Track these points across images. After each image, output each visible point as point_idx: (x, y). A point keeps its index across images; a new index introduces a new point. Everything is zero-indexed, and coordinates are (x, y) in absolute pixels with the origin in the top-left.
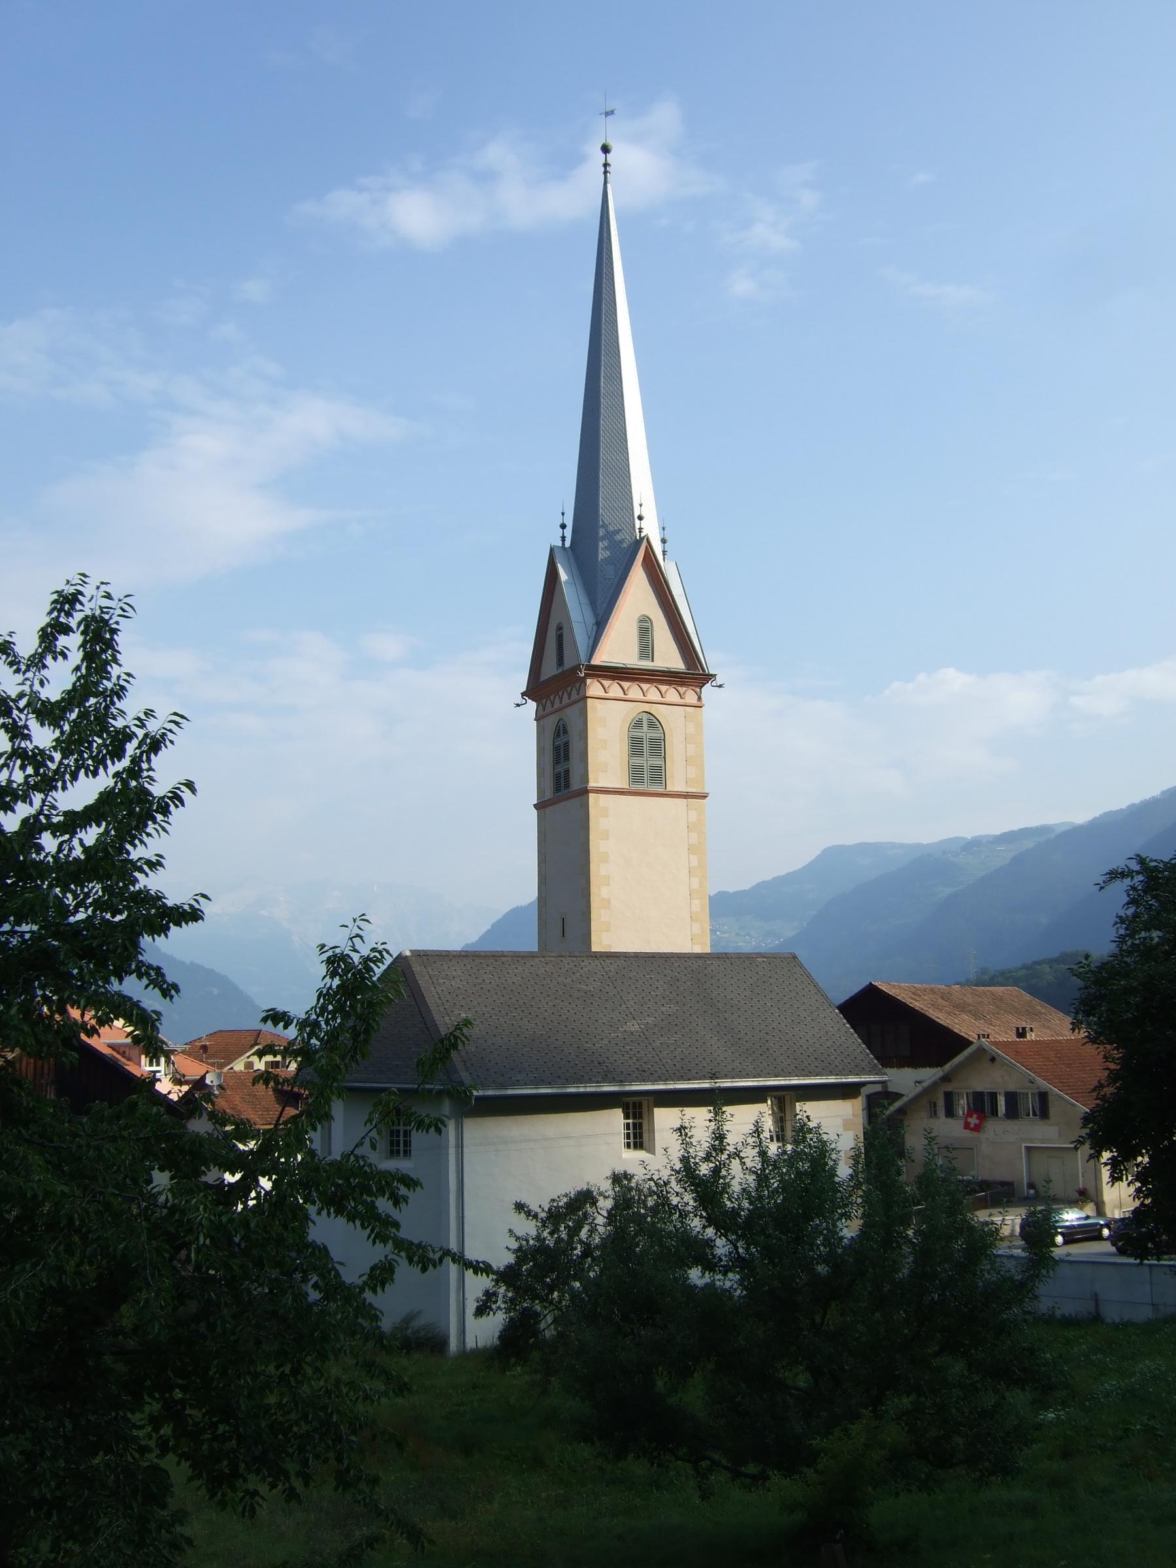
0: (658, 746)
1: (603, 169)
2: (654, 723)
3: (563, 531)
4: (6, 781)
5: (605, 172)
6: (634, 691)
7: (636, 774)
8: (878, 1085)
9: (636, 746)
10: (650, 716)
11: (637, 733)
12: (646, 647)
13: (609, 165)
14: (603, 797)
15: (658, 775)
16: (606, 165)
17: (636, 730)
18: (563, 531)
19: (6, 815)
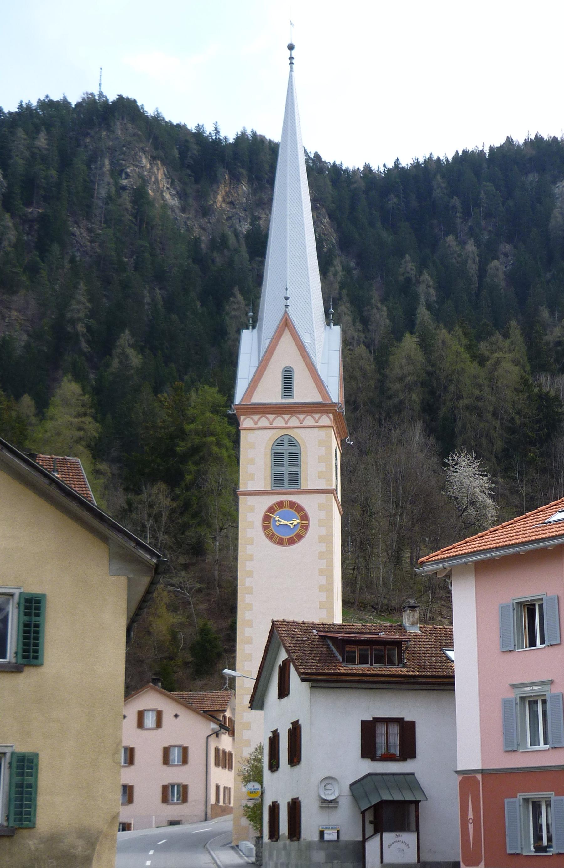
0: (295, 459)
1: (289, 62)
2: (292, 443)
3: (291, 52)
4: (552, 393)
5: (291, 63)
6: (279, 421)
7: (277, 479)
8: (417, 859)
9: (277, 460)
10: (289, 436)
11: (279, 450)
12: (288, 390)
13: (293, 58)
14: (249, 498)
15: (295, 479)
16: (291, 58)
17: (276, 468)
18: (291, 52)
19: (398, 159)
